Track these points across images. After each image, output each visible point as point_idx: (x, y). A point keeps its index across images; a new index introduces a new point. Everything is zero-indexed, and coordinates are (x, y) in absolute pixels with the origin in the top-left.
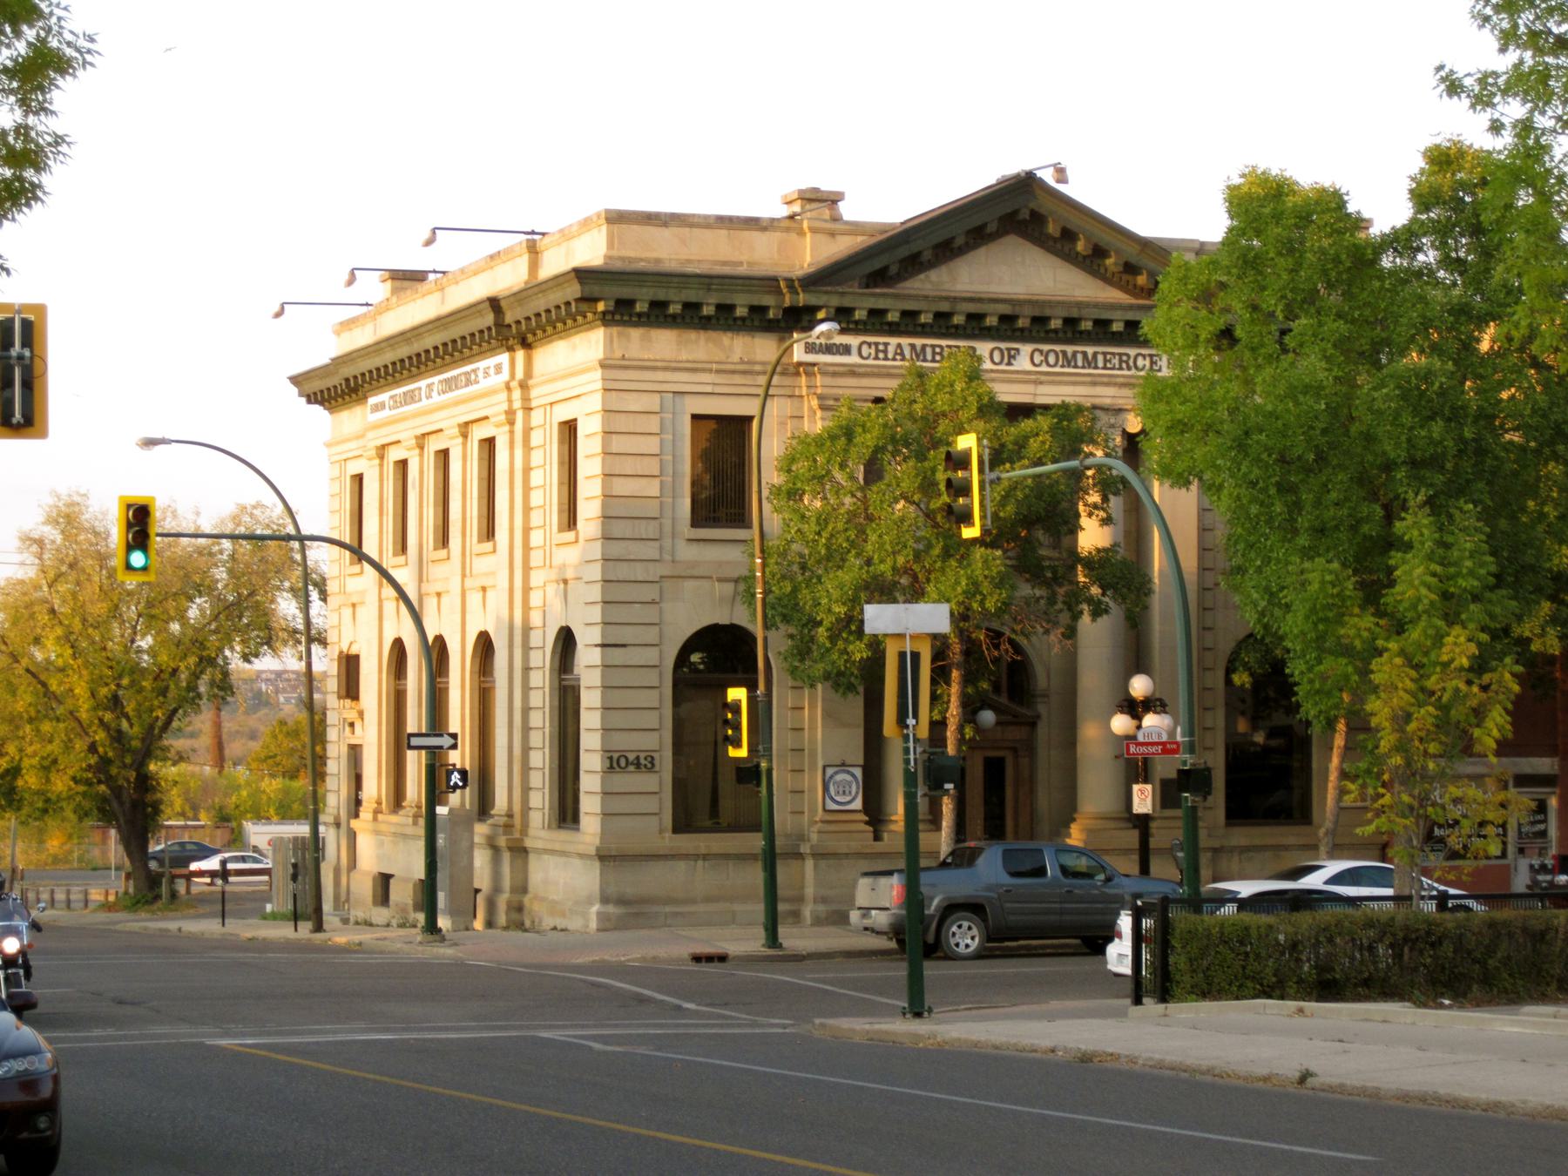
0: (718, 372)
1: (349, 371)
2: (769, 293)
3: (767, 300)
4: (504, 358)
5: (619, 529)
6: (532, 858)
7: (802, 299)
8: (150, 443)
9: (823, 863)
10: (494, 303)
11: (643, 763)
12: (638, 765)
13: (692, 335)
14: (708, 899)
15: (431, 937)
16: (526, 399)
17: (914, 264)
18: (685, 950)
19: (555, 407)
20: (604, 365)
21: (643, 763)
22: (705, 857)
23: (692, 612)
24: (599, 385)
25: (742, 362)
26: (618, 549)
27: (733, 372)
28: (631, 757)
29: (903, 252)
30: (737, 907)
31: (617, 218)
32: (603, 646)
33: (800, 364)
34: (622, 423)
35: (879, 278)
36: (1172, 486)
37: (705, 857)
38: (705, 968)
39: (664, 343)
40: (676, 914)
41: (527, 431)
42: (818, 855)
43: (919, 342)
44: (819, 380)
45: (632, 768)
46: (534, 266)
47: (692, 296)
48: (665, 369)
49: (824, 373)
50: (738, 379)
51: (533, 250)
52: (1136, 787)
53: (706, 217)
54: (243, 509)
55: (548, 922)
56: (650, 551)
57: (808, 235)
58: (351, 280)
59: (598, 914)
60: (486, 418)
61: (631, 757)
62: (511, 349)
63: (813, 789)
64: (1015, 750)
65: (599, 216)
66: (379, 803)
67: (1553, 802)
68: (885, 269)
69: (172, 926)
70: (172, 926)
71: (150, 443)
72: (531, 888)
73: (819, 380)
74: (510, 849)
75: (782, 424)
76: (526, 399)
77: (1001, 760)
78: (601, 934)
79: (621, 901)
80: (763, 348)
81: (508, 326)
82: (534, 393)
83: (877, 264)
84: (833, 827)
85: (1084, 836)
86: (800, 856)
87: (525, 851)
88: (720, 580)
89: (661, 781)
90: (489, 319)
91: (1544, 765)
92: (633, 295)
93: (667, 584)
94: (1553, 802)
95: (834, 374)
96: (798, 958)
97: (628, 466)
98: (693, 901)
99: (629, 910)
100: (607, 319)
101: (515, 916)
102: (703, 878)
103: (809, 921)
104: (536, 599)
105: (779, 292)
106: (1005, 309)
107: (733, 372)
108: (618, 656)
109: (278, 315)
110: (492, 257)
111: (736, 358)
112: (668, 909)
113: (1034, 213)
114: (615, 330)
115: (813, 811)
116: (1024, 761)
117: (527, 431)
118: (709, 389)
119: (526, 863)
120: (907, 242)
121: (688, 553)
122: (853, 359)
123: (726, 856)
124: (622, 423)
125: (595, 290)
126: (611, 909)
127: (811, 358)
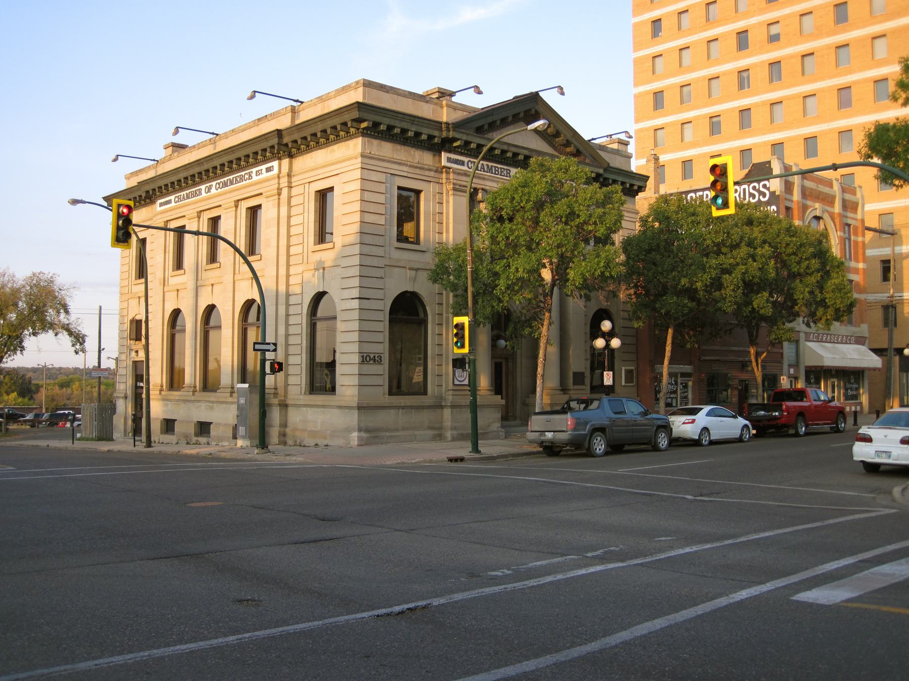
0: (410, 166)
1: (149, 187)
2: (437, 129)
3: (436, 133)
4: (275, 164)
5: (368, 239)
6: (290, 409)
7: (451, 134)
8: (75, 202)
9: (455, 410)
10: (279, 133)
11: (376, 360)
12: (375, 361)
13: (399, 147)
14: (404, 429)
15: (264, 451)
16: (290, 182)
17: (492, 127)
18: (444, 456)
19: (311, 184)
20: (362, 156)
21: (376, 360)
22: (403, 408)
23: (396, 286)
24: (359, 165)
25: (418, 163)
26: (367, 250)
27: (416, 167)
28: (372, 356)
29: (490, 120)
30: (417, 432)
31: (368, 84)
32: (359, 298)
33: (444, 167)
34: (369, 186)
35: (479, 130)
36: (876, 177)
37: (403, 408)
38: (453, 464)
39: (387, 149)
40: (391, 436)
41: (290, 197)
42: (453, 407)
43: (490, 164)
44: (451, 176)
45: (372, 362)
46: (293, 119)
47: (405, 125)
48: (389, 161)
49: (454, 172)
50: (418, 171)
51: (293, 110)
52: (605, 373)
53: (405, 91)
54: (34, 274)
55: (312, 442)
56: (379, 251)
57: (445, 109)
58: (176, 131)
59: (358, 437)
60: (261, 194)
61: (372, 356)
62: (280, 159)
63: (447, 374)
64: (506, 359)
65: (357, 82)
66: (162, 386)
67: (690, 383)
68: (482, 126)
69: (42, 443)
70: (42, 443)
71: (75, 202)
72: (289, 424)
73: (451, 176)
74: (280, 405)
75: (434, 196)
76: (290, 182)
77: (501, 364)
78: (366, 449)
79: (367, 430)
80: (426, 158)
81: (285, 144)
82: (293, 179)
83: (480, 123)
84: (457, 393)
85: (549, 397)
86: (442, 407)
87: (286, 406)
88: (410, 269)
89: (383, 369)
90: (275, 141)
91: (688, 368)
92: (378, 120)
93: (387, 269)
94: (690, 383)
95: (459, 174)
96: (491, 459)
97: (372, 208)
98: (397, 430)
99: (372, 435)
100: (365, 133)
101: (282, 439)
102: (402, 418)
103: (449, 439)
104: (292, 280)
105: (441, 130)
106: (526, 153)
107: (416, 167)
108: (367, 304)
109: (115, 160)
110: (259, 120)
111: (416, 161)
112: (388, 434)
113: (536, 111)
114: (366, 139)
115: (447, 385)
116: (510, 364)
117: (290, 197)
118: (405, 174)
119: (286, 412)
120: (492, 115)
121: (397, 255)
122: (465, 168)
123: (411, 407)
124: (369, 186)
125: (365, 115)
126: (363, 434)
127: (449, 165)
